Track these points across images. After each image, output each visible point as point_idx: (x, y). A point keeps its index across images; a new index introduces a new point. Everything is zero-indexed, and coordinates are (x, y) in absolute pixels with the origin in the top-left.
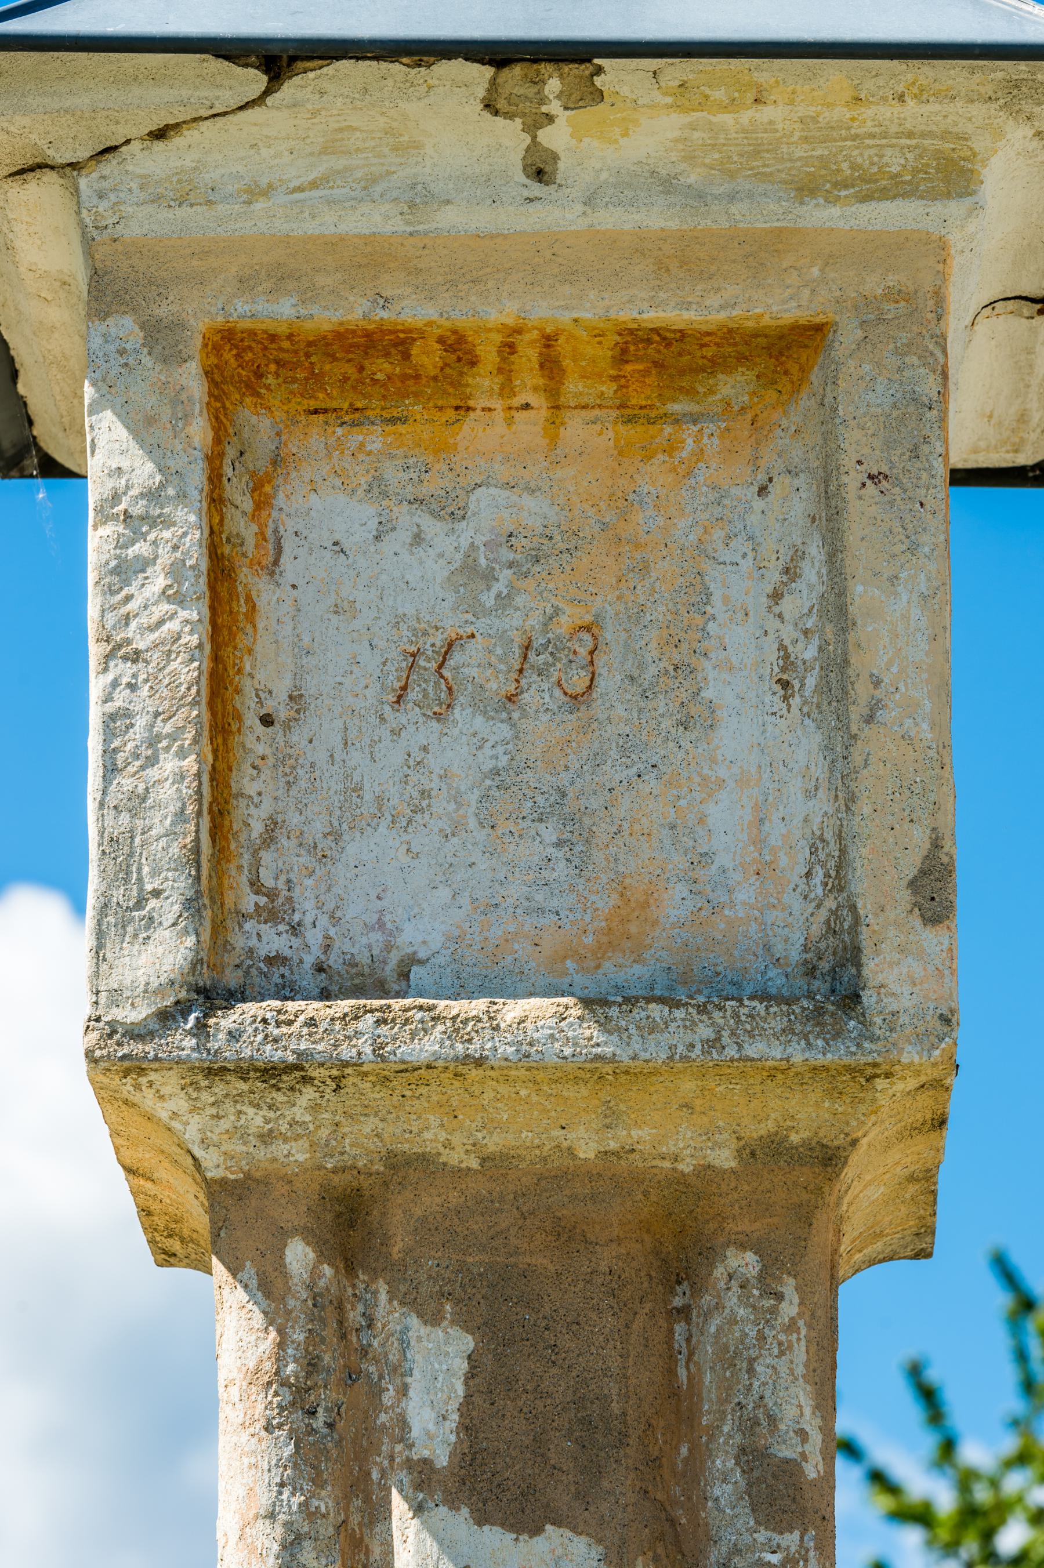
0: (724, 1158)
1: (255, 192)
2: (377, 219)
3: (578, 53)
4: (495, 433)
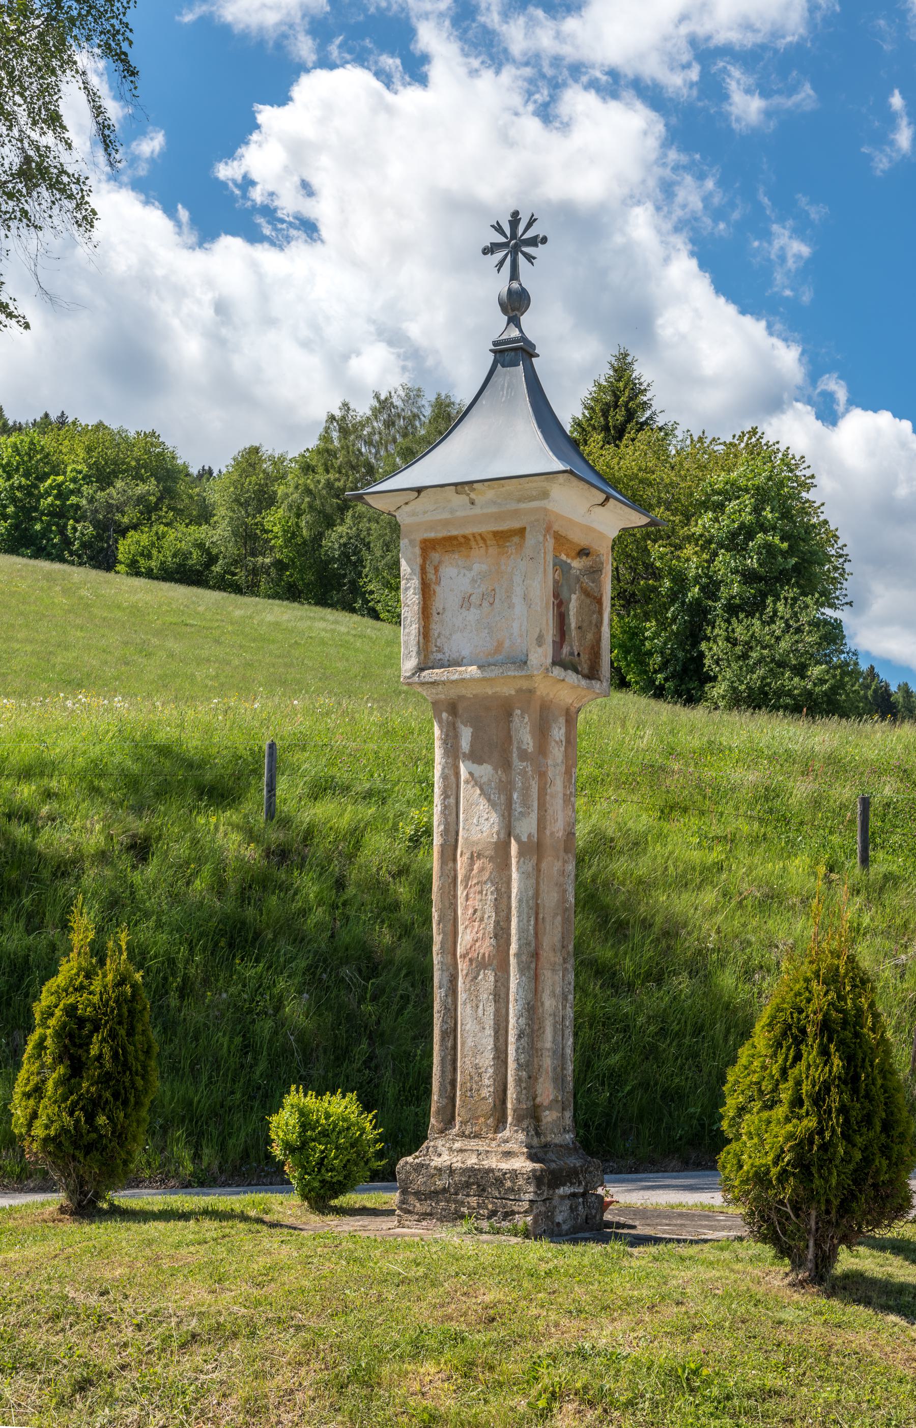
0: (513, 692)
2: (446, 515)
4: (477, 552)
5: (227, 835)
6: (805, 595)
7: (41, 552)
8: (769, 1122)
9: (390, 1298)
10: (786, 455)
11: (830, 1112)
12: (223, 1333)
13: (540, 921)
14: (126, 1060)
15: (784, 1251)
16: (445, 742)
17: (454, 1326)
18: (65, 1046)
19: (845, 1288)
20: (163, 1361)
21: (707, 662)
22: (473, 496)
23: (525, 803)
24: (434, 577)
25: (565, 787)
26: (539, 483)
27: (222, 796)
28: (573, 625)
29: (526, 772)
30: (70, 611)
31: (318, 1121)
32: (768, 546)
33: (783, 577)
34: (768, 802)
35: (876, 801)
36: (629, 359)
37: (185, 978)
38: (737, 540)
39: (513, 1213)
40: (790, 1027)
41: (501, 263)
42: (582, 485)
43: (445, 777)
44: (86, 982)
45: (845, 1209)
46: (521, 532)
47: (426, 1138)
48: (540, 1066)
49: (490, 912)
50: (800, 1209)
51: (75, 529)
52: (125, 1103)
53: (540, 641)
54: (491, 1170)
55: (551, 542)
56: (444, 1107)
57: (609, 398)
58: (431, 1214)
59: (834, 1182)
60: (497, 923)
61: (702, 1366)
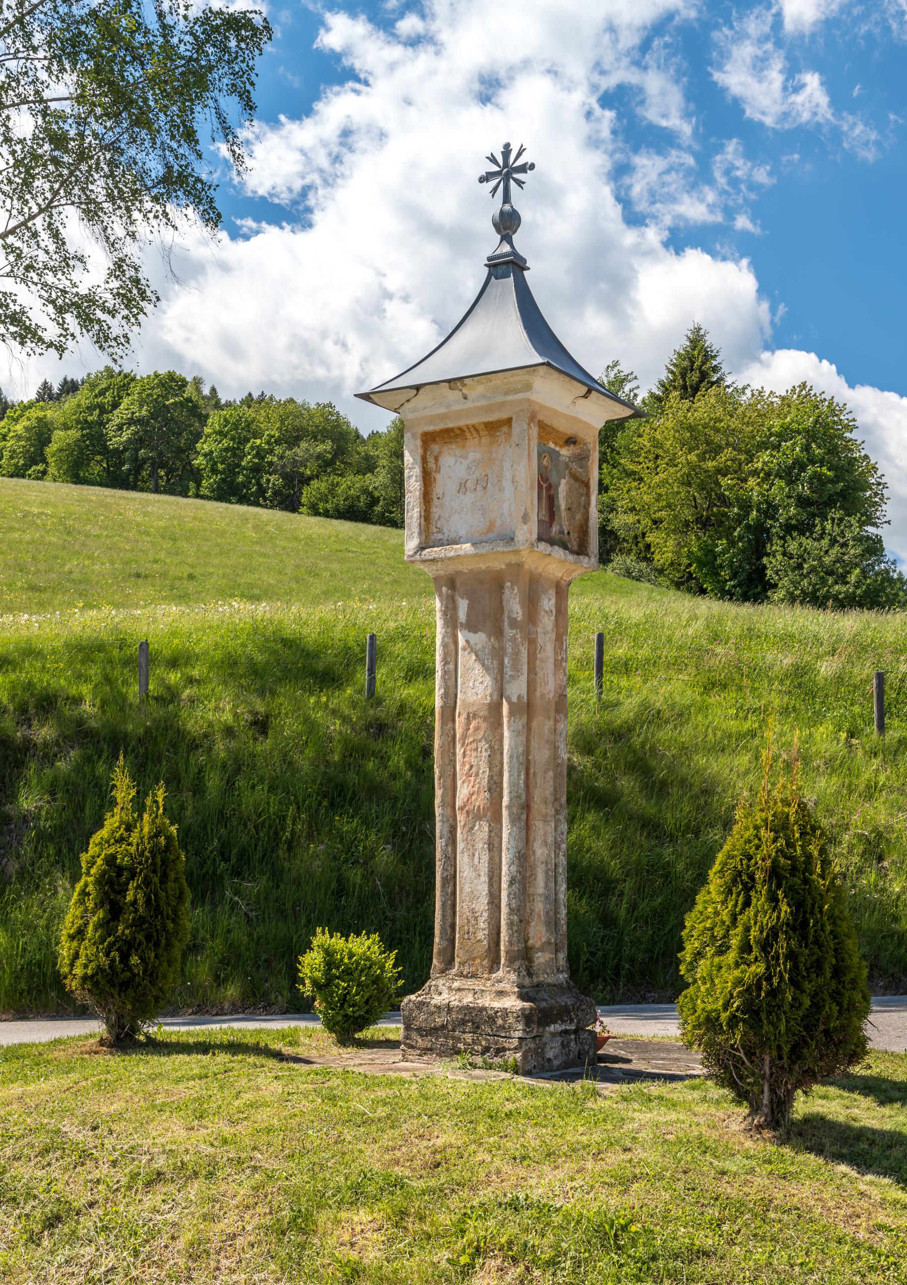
0: (503, 567)
1: (425, 408)
2: (442, 410)
3: (461, 379)
5: (331, 713)
6: (849, 515)
7: (243, 500)
8: (720, 968)
9: (349, 1138)
10: (831, 404)
11: (778, 959)
12: (186, 1173)
13: (531, 775)
14: (158, 905)
15: (742, 1096)
16: (445, 613)
17: (398, 1170)
18: (106, 893)
19: (800, 1134)
20: (127, 1200)
21: (769, 572)
22: (465, 391)
23: (515, 666)
24: (434, 466)
25: (556, 653)
26: (521, 377)
27: (333, 680)
28: (563, 507)
29: (516, 639)
30: (257, 543)
31: (342, 960)
32: (816, 476)
33: (830, 502)
34: (800, 680)
35: (890, 677)
36: (702, 332)
37: (293, 832)
38: (790, 474)
39: (504, 1049)
40: (740, 874)
41: (495, 190)
42: (562, 377)
43: (445, 646)
44: (126, 834)
45: (796, 1053)
46: (509, 422)
47: (428, 977)
48: (532, 911)
49: (484, 768)
50: (754, 1054)
51: (268, 481)
52: (157, 944)
53: (525, 519)
54: (484, 1009)
55: (535, 431)
56: (445, 949)
57: (686, 363)
58: (431, 1049)
59: (783, 1028)
60: (491, 777)
61: (631, 1221)
